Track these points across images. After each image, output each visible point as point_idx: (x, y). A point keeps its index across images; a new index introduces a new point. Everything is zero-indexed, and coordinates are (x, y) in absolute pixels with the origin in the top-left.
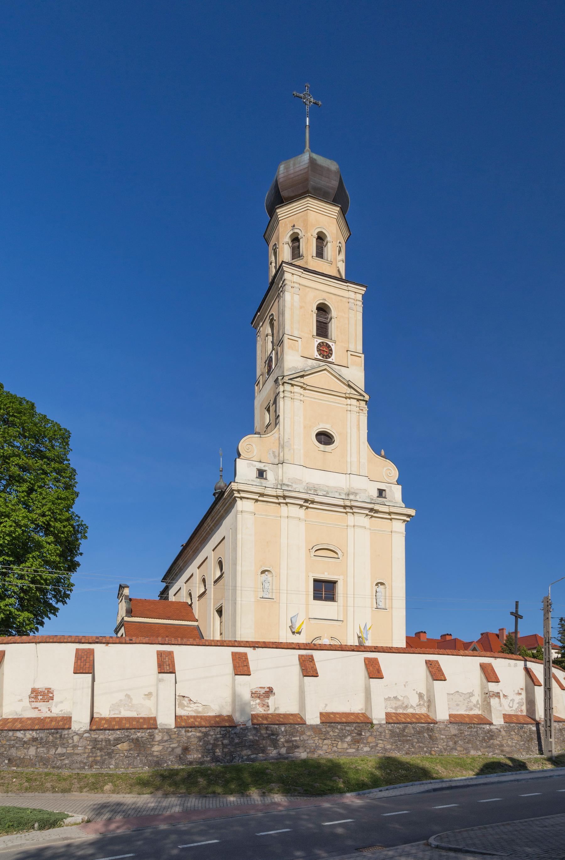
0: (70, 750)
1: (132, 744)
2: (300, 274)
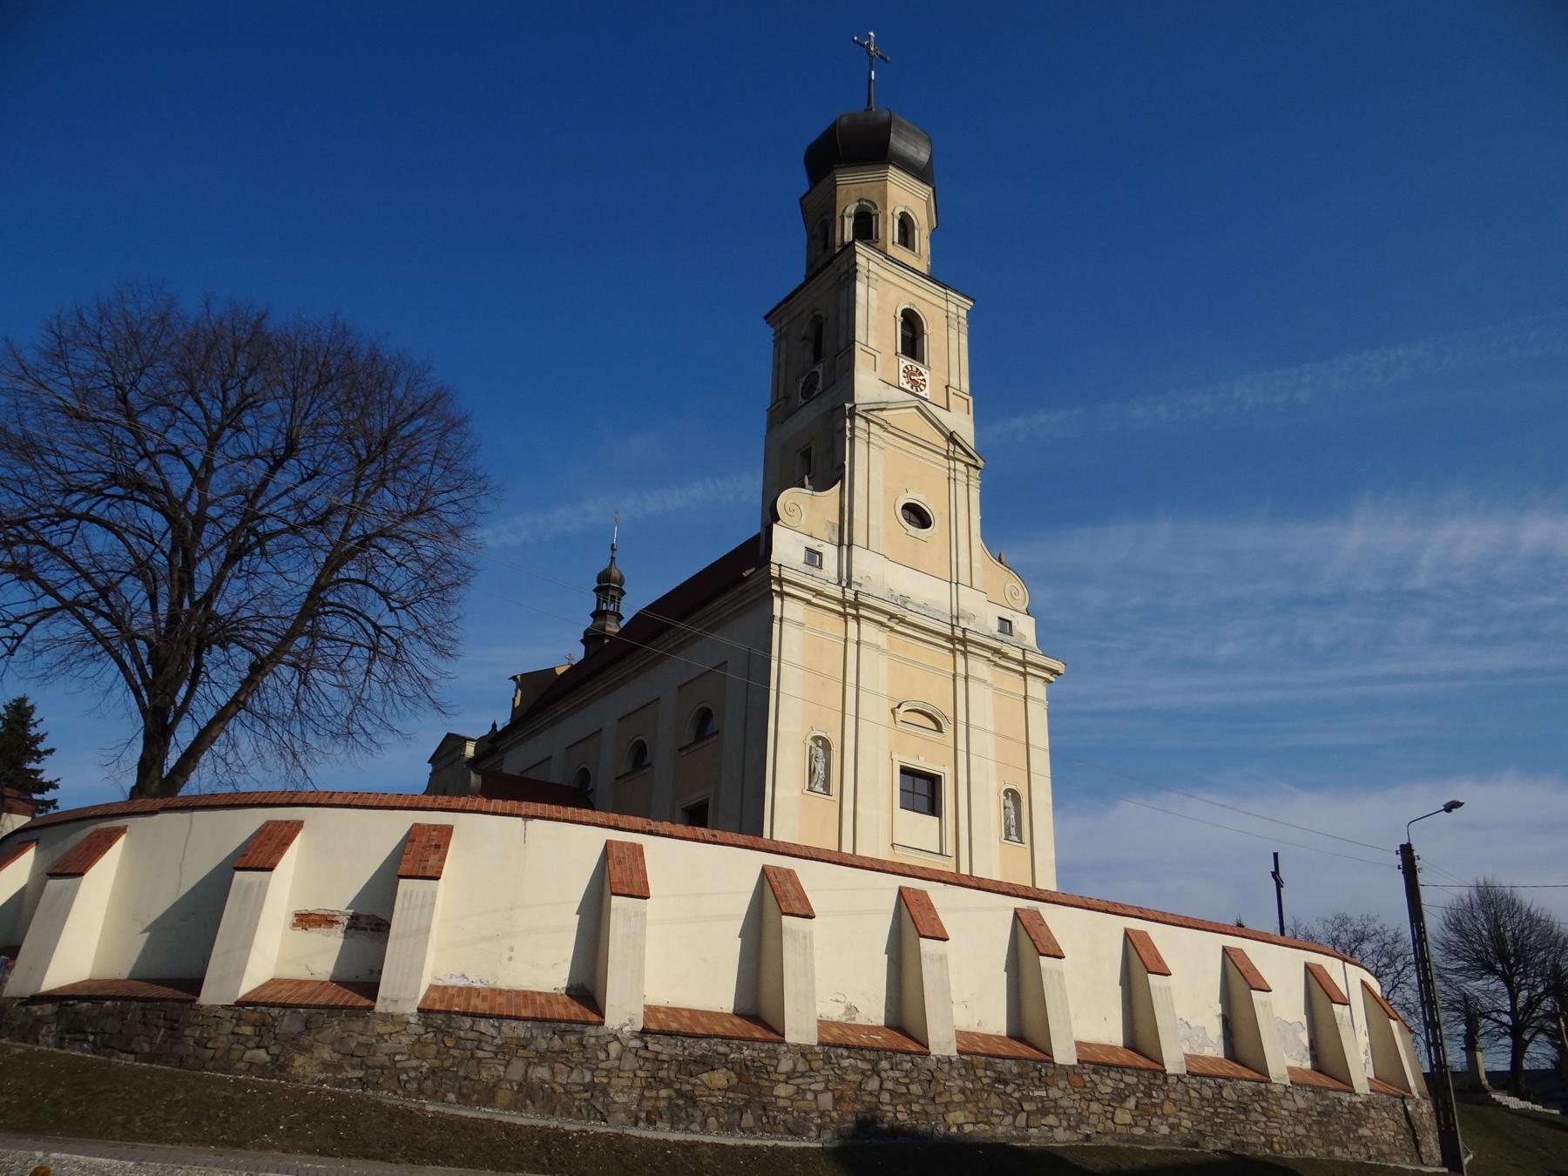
1: (732, 1074)
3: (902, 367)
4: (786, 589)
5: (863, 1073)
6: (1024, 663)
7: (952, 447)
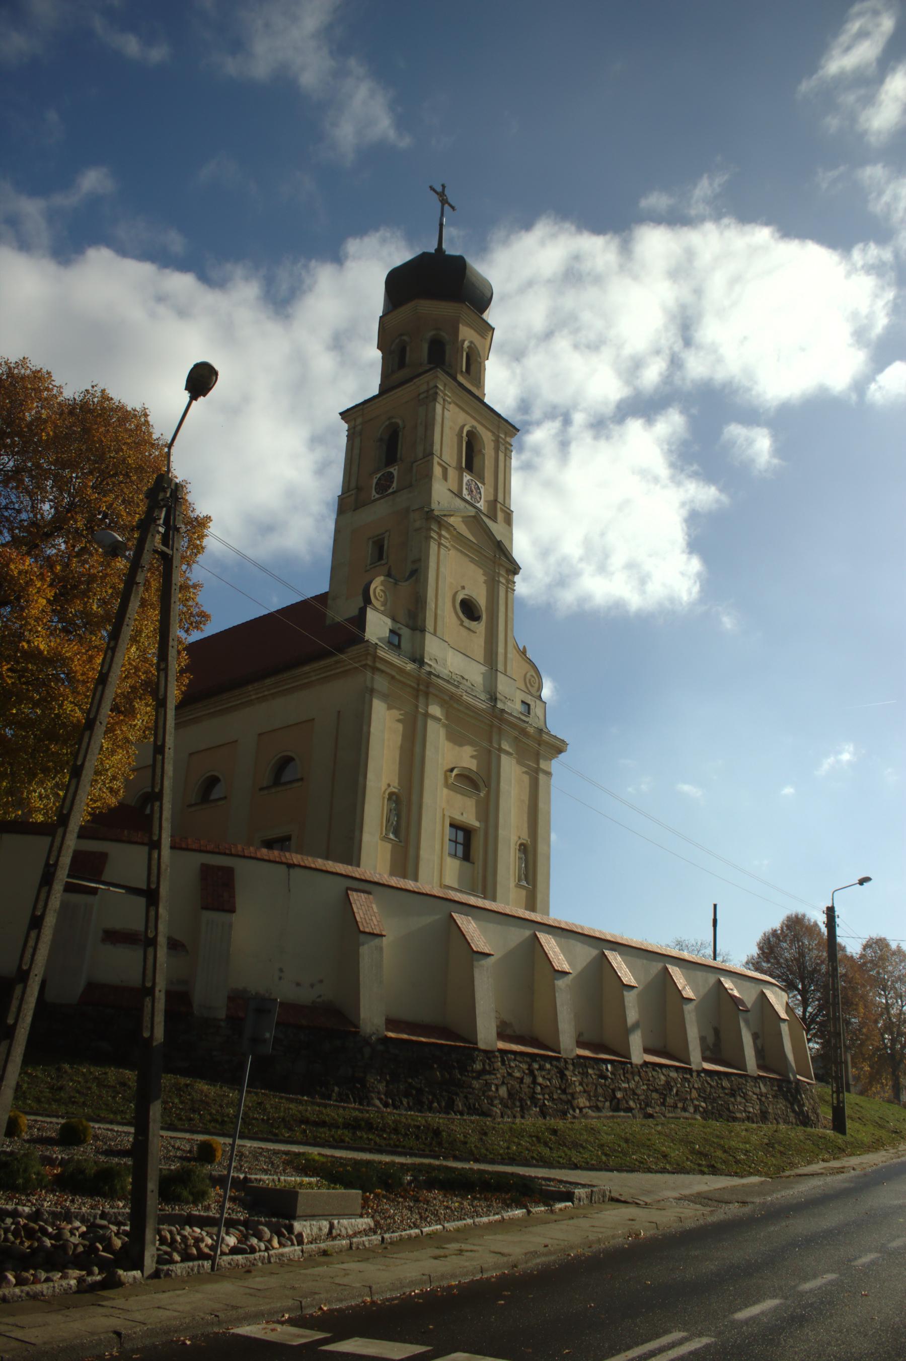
4: (378, 665)
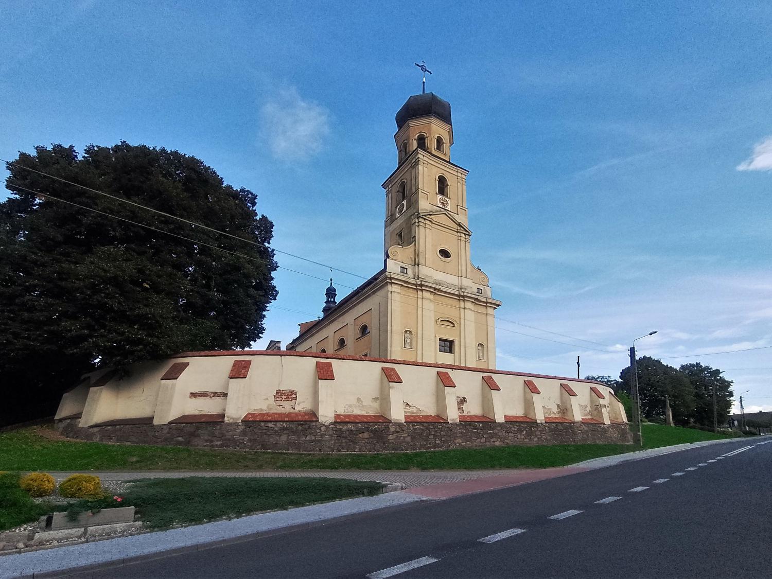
0: (318, 438)
2: (428, 156)
3: (438, 198)
5: (422, 430)
6: (486, 303)
7: (459, 228)
